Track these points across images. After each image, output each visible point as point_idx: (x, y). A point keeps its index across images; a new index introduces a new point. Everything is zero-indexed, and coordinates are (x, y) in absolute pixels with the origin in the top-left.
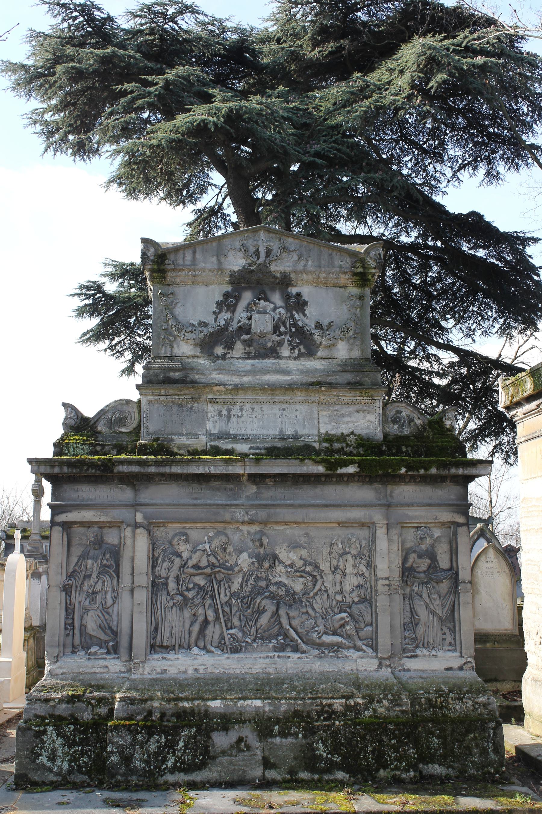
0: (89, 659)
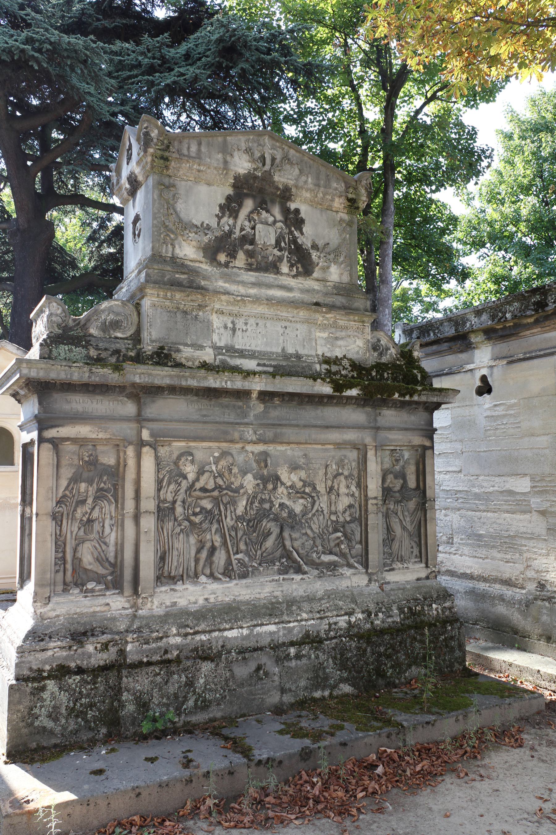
0: (86, 597)
